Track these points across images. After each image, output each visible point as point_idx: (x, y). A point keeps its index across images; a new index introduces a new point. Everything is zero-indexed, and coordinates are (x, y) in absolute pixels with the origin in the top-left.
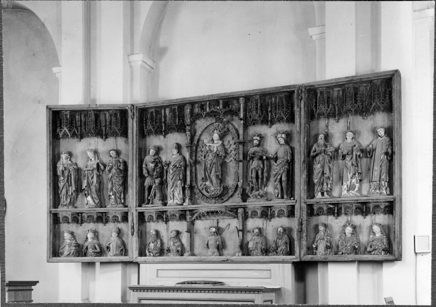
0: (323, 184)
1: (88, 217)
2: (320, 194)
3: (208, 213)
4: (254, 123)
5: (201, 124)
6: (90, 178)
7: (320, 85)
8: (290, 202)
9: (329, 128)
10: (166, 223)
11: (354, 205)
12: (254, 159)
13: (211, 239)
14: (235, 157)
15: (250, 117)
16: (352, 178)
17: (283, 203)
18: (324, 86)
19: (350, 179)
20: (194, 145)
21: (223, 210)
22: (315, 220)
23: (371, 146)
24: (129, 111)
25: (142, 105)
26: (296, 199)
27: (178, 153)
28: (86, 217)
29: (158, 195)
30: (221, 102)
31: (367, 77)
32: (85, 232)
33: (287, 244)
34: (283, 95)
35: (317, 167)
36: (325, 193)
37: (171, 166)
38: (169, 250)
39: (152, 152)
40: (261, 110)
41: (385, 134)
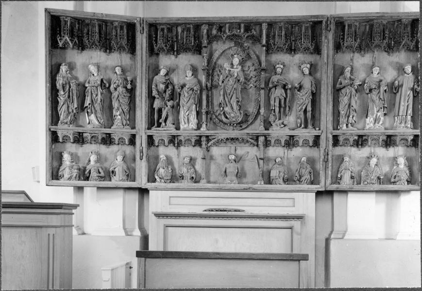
0: (348, 117)
1: (92, 137)
2: (345, 125)
3: (227, 139)
4: (279, 50)
5: (219, 47)
6: (94, 96)
7: (349, 17)
8: (316, 132)
9: (355, 61)
10: (177, 149)
11: (381, 137)
12: (277, 87)
13: (230, 167)
14: (255, 84)
15: (274, 45)
16: (378, 112)
17: (309, 133)
18: (352, 19)
19: (376, 111)
20: (211, 69)
21: (245, 137)
22: (338, 150)
23: (397, 82)
24: (138, 25)
25: (152, 20)
26: (322, 128)
27: (192, 75)
28: (89, 138)
29: (170, 119)
30: (242, 25)
31: (398, 15)
32: (90, 153)
33: (310, 173)
34: (308, 25)
35: (344, 100)
36: (350, 125)
37: (185, 89)
38: (182, 177)
39: (163, 72)
40: (286, 37)
41: (160, 71)
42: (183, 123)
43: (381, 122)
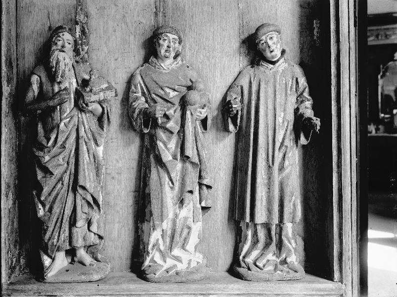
43: (193, 240)
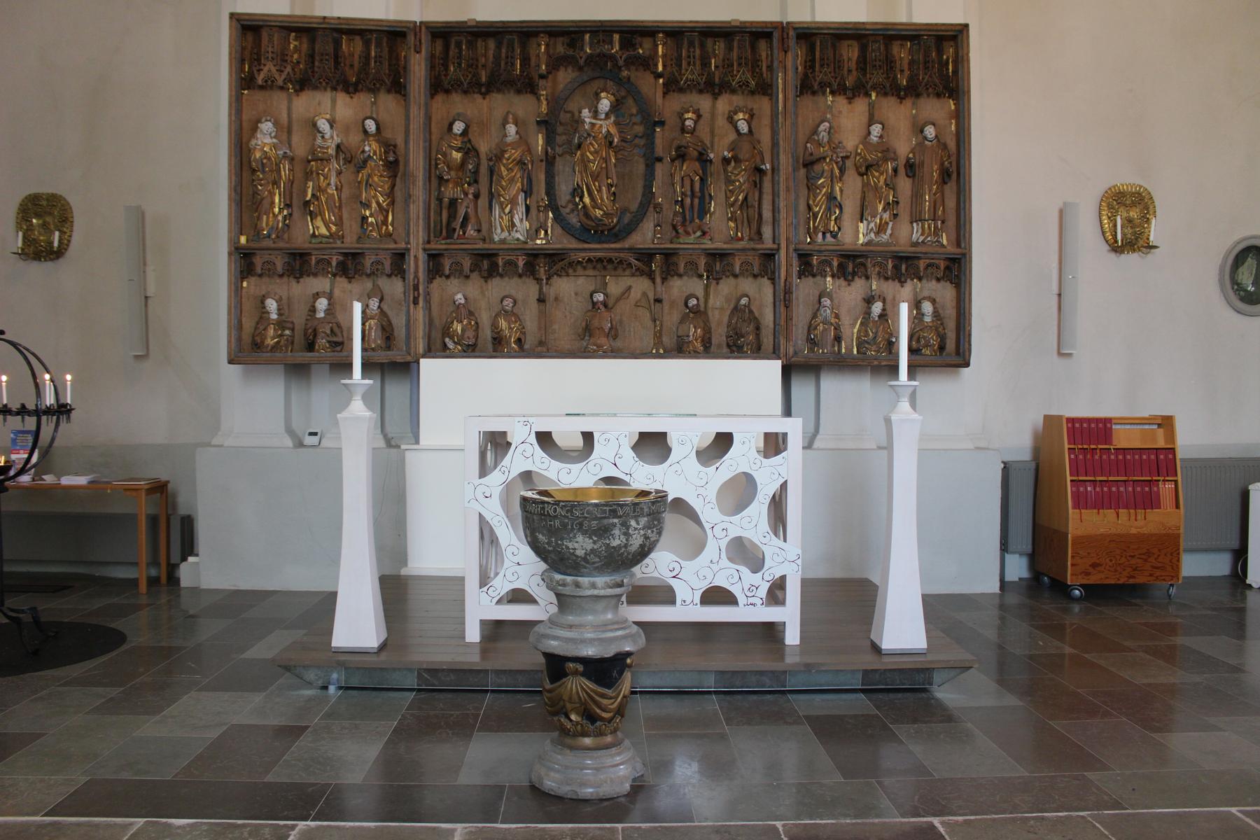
42: (499, 230)
43: (889, 231)
